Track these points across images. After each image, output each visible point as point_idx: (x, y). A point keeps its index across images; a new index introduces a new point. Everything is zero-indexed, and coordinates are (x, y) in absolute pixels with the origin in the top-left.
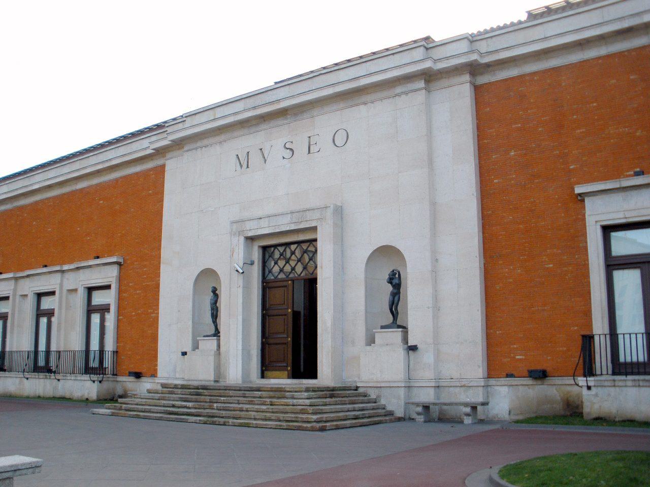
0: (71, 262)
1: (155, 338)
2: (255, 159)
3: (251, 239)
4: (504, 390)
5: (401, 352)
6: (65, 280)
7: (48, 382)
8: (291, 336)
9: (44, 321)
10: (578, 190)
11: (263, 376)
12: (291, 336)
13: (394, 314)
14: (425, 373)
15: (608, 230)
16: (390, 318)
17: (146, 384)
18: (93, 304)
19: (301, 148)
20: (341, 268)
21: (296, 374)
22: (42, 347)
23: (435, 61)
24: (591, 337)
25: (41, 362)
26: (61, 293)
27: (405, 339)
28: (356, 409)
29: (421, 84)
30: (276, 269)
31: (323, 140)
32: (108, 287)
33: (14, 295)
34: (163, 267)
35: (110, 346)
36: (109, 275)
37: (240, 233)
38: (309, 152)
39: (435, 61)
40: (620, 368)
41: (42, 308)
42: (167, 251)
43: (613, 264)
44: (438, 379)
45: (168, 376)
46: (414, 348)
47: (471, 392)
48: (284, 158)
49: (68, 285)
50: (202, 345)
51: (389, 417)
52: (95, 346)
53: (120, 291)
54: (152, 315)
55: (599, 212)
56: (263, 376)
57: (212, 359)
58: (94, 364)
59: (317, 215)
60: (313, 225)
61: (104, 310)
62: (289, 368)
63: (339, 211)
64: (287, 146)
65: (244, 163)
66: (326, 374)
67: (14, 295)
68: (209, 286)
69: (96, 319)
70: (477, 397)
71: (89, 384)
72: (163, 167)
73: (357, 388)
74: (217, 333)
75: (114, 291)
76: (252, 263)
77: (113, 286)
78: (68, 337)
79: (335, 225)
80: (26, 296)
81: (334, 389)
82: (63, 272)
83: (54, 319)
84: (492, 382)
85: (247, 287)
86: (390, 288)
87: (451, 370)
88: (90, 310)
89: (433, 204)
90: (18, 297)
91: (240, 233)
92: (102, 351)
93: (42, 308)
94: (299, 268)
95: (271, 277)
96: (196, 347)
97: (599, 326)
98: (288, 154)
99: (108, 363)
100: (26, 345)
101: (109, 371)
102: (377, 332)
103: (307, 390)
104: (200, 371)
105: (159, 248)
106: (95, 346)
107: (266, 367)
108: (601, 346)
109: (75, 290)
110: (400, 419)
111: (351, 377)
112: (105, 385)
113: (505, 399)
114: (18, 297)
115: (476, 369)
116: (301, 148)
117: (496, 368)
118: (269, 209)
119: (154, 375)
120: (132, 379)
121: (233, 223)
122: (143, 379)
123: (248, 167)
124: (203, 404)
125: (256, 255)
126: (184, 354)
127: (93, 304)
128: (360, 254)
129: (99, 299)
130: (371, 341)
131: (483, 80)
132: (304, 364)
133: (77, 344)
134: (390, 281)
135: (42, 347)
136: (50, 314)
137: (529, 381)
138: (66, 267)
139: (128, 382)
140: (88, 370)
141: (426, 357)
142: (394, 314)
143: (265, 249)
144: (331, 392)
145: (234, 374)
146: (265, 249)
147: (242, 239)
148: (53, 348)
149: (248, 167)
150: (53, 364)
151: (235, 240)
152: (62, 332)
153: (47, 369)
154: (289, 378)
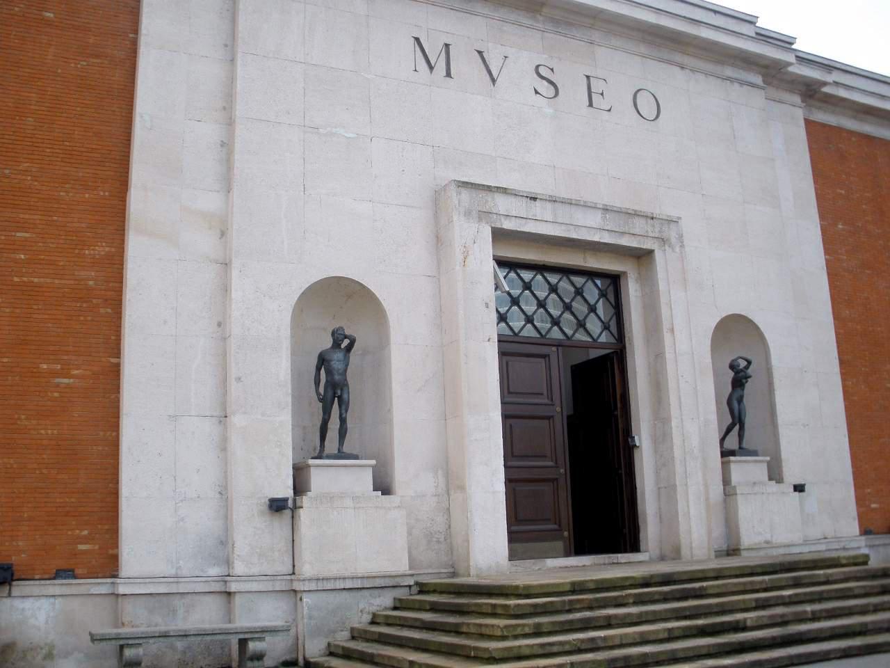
34: (137, 249)
38: (591, 105)
45: (173, 572)
46: (799, 488)
48: (537, 92)
54: (57, 380)
60: (647, 245)
62: (566, 534)
64: (542, 71)
96: (300, 487)
98: (544, 87)
116: (574, 93)
122: (19, 588)
123: (448, 74)
126: (277, 506)
149: (448, 74)
154: (567, 554)
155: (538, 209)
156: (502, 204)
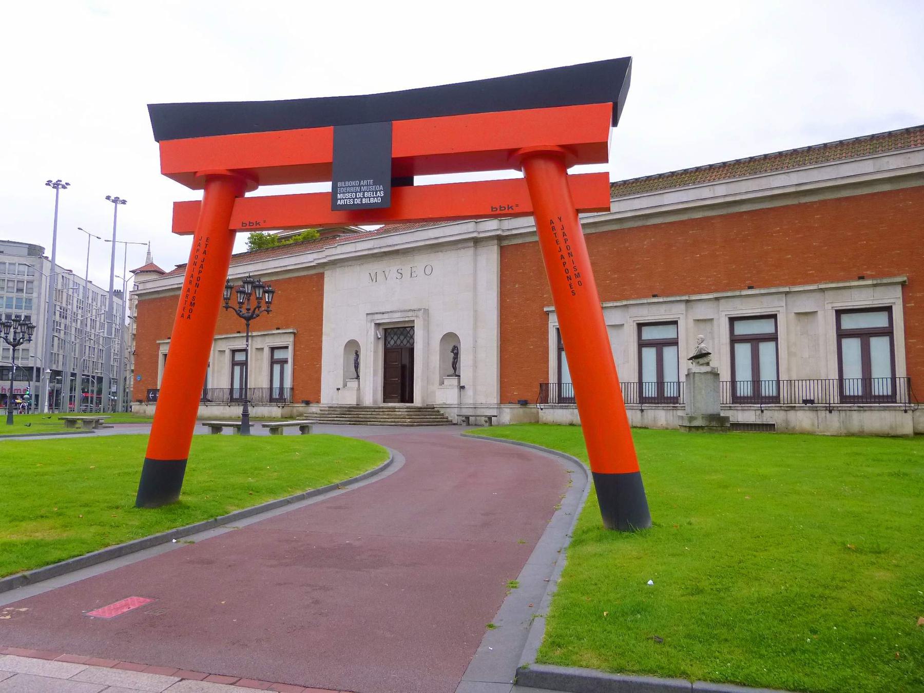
1: (318, 381)
2: (380, 277)
3: (378, 325)
4: (508, 411)
5: (456, 390)
8: (399, 378)
10: (545, 309)
11: (384, 402)
12: (399, 378)
13: (455, 368)
16: (452, 371)
17: (314, 409)
19: (406, 273)
20: (427, 344)
21: (403, 400)
23: (479, 233)
27: (459, 382)
28: (432, 416)
29: (472, 244)
30: (392, 342)
31: (419, 270)
32: (287, 347)
34: (324, 338)
36: (289, 340)
39: (479, 233)
41: (843, 327)
46: (463, 387)
50: (348, 384)
51: (450, 423)
52: (276, 384)
56: (384, 402)
57: (355, 392)
61: (283, 362)
63: (426, 311)
66: (418, 401)
68: (353, 348)
69: (277, 368)
70: (494, 412)
74: (358, 377)
75: (291, 349)
79: (424, 320)
81: (421, 408)
86: (452, 355)
87: (481, 399)
88: (273, 362)
89: (475, 311)
90: (254, 350)
91: (372, 320)
92: (282, 389)
93: (843, 327)
94: (405, 342)
96: (345, 385)
97: (553, 379)
98: (399, 276)
99: (287, 394)
100: (225, 384)
102: (334, 263)
103: (407, 408)
104: (349, 399)
105: (322, 325)
106: (276, 384)
107: (387, 397)
110: (454, 424)
111: (430, 402)
113: (508, 414)
115: (494, 399)
116: (406, 273)
117: (504, 398)
119: (318, 402)
120: (303, 405)
124: (354, 415)
126: (338, 389)
128: (437, 337)
129: (279, 355)
130: (442, 383)
131: (505, 243)
132: (406, 395)
133: (265, 384)
134: (452, 351)
137: (518, 406)
139: (300, 407)
140: (272, 400)
141: (469, 392)
142: (455, 368)
143: (386, 330)
144: (419, 409)
145: (368, 401)
146: (386, 330)
147: (373, 324)
151: (369, 324)
155: (386, 316)
156: (377, 317)
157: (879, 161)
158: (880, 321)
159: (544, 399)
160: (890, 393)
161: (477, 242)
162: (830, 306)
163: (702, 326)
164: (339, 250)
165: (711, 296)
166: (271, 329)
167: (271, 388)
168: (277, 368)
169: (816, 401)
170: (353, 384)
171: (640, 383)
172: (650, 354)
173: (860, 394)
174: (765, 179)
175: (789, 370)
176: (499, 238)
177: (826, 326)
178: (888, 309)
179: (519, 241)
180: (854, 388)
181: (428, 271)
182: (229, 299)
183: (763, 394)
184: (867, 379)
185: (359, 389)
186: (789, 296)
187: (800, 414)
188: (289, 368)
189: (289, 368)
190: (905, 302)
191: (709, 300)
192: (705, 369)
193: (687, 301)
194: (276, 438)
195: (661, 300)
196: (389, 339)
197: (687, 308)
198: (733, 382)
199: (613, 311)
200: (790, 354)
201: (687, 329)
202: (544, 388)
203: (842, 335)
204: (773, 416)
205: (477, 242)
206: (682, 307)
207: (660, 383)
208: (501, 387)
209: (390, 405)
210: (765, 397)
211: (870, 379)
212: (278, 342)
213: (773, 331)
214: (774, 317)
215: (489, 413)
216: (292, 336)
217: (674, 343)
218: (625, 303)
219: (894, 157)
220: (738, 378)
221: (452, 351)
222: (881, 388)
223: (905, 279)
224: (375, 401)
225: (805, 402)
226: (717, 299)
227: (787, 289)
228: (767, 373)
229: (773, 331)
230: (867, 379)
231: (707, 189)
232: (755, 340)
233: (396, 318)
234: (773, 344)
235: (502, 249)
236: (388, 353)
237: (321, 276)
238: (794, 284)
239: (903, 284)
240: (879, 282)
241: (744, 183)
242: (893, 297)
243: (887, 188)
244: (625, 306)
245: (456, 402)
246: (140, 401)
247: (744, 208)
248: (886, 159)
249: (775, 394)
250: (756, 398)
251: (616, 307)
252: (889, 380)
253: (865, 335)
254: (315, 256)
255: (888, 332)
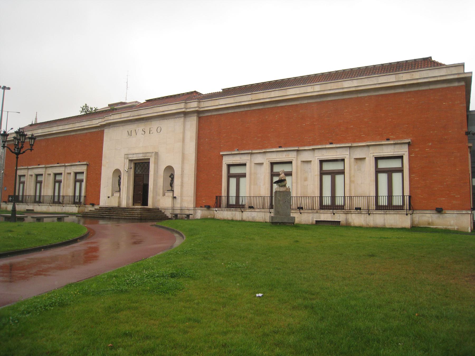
0: (68, 163)
2: (133, 133)
3: (131, 161)
5: (170, 199)
6: (66, 170)
7: (59, 207)
8: (141, 191)
9: (57, 185)
10: (221, 153)
12: (141, 191)
14: (178, 205)
15: (229, 166)
16: (170, 188)
18: (470, 110)
19: (147, 132)
20: (156, 171)
22: (56, 194)
24: (221, 197)
25: (56, 200)
26: (45, 175)
27: (173, 194)
29: (183, 115)
31: (154, 130)
32: (83, 173)
33: (45, 174)
35: (83, 194)
36: (84, 169)
37: (127, 158)
39: (186, 109)
40: (229, 206)
42: (105, 161)
43: (230, 176)
44: (181, 207)
47: (190, 211)
49: (68, 172)
52: (77, 194)
53: (87, 175)
55: (227, 160)
57: (117, 199)
58: (77, 200)
59: (150, 155)
61: (81, 181)
63: (157, 154)
65: (130, 134)
67: (45, 174)
68: (117, 173)
69: (78, 184)
70: (191, 212)
71: (75, 208)
72: (103, 131)
73: (159, 209)
74: (120, 191)
76: (131, 168)
77: (85, 173)
78: (67, 190)
80: (50, 174)
82: (65, 166)
83: (62, 184)
84: (197, 209)
85: (129, 176)
86: (170, 179)
87: (185, 205)
88: (76, 181)
90: (46, 175)
91: (127, 158)
92: (80, 196)
95: (137, 173)
96: (113, 195)
97: (224, 193)
99: (82, 200)
100: (50, 193)
101: (82, 203)
104: (114, 203)
105: (101, 160)
106: (77, 194)
108: (224, 200)
109: (70, 173)
111: (157, 206)
112: (81, 208)
113: (200, 213)
114: (46, 175)
116: (147, 132)
117: (198, 204)
118: (137, 151)
119: (99, 205)
120: (91, 206)
121: (125, 155)
125: (132, 166)
126: (109, 197)
127: (470, 110)
128: (162, 168)
129: (79, 177)
130: (164, 195)
132: (145, 202)
133: (71, 193)
134: (170, 177)
135: (56, 194)
136: (60, 182)
138: (66, 164)
140: (75, 203)
141: (178, 200)
144: (149, 210)
145: (124, 204)
146: (135, 164)
148: (61, 194)
150: (61, 201)
151: (126, 160)
152: (65, 189)
153: (59, 203)
155: (135, 156)
157: (397, 76)
158: (396, 164)
159: (218, 205)
160: (401, 204)
161: (186, 114)
162: (372, 155)
163: (359, 162)
164: (112, 117)
165: (44, 166)
166: (75, 162)
167: (74, 196)
168: (78, 184)
169: (362, 209)
170: (117, 195)
171: (377, 197)
172: (327, 179)
173: (387, 204)
174: (340, 83)
175: (350, 190)
176: (198, 112)
177: (369, 166)
178: (401, 157)
179: (209, 114)
180: (383, 201)
181: (159, 130)
182: (33, 145)
183: (337, 204)
184: (390, 196)
185: (120, 197)
186: (351, 149)
187: (353, 215)
188: (84, 184)
189: (84, 184)
190: (410, 154)
191: (309, 150)
192: (282, 189)
193: (298, 151)
194: (60, 223)
195: (283, 149)
196: (137, 168)
197: (297, 155)
198: (228, 196)
199: (259, 155)
200: (351, 181)
201: (297, 166)
202: (218, 198)
203: (378, 171)
204: (340, 217)
205: (186, 114)
206: (294, 154)
207: (333, 197)
208: (196, 198)
209: (136, 207)
210: (381, 206)
211: (392, 196)
212: (78, 169)
213: (401, 166)
214: (343, 160)
215: (188, 212)
216: (407, 146)
217: (342, 172)
218: (263, 151)
219: (405, 74)
220: (380, 194)
221: (170, 177)
222: (397, 201)
223: (409, 141)
224: (127, 204)
225: (357, 209)
226: (313, 150)
227: (350, 145)
228: (339, 192)
229: (401, 166)
230: (390, 196)
231: (310, 87)
232: (333, 174)
233: (141, 157)
234: (343, 176)
235: (200, 118)
236: (136, 176)
237: (103, 132)
238: (354, 141)
239: (409, 144)
240: (397, 142)
241: (329, 84)
242: (404, 151)
243: (402, 90)
244: (265, 152)
245: (170, 206)
246: (6, 202)
247: (329, 99)
248: (402, 75)
249: (343, 204)
250: (333, 207)
251: (259, 153)
252: (401, 197)
253: (390, 172)
254: (100, 120)
255: (400, 170)
